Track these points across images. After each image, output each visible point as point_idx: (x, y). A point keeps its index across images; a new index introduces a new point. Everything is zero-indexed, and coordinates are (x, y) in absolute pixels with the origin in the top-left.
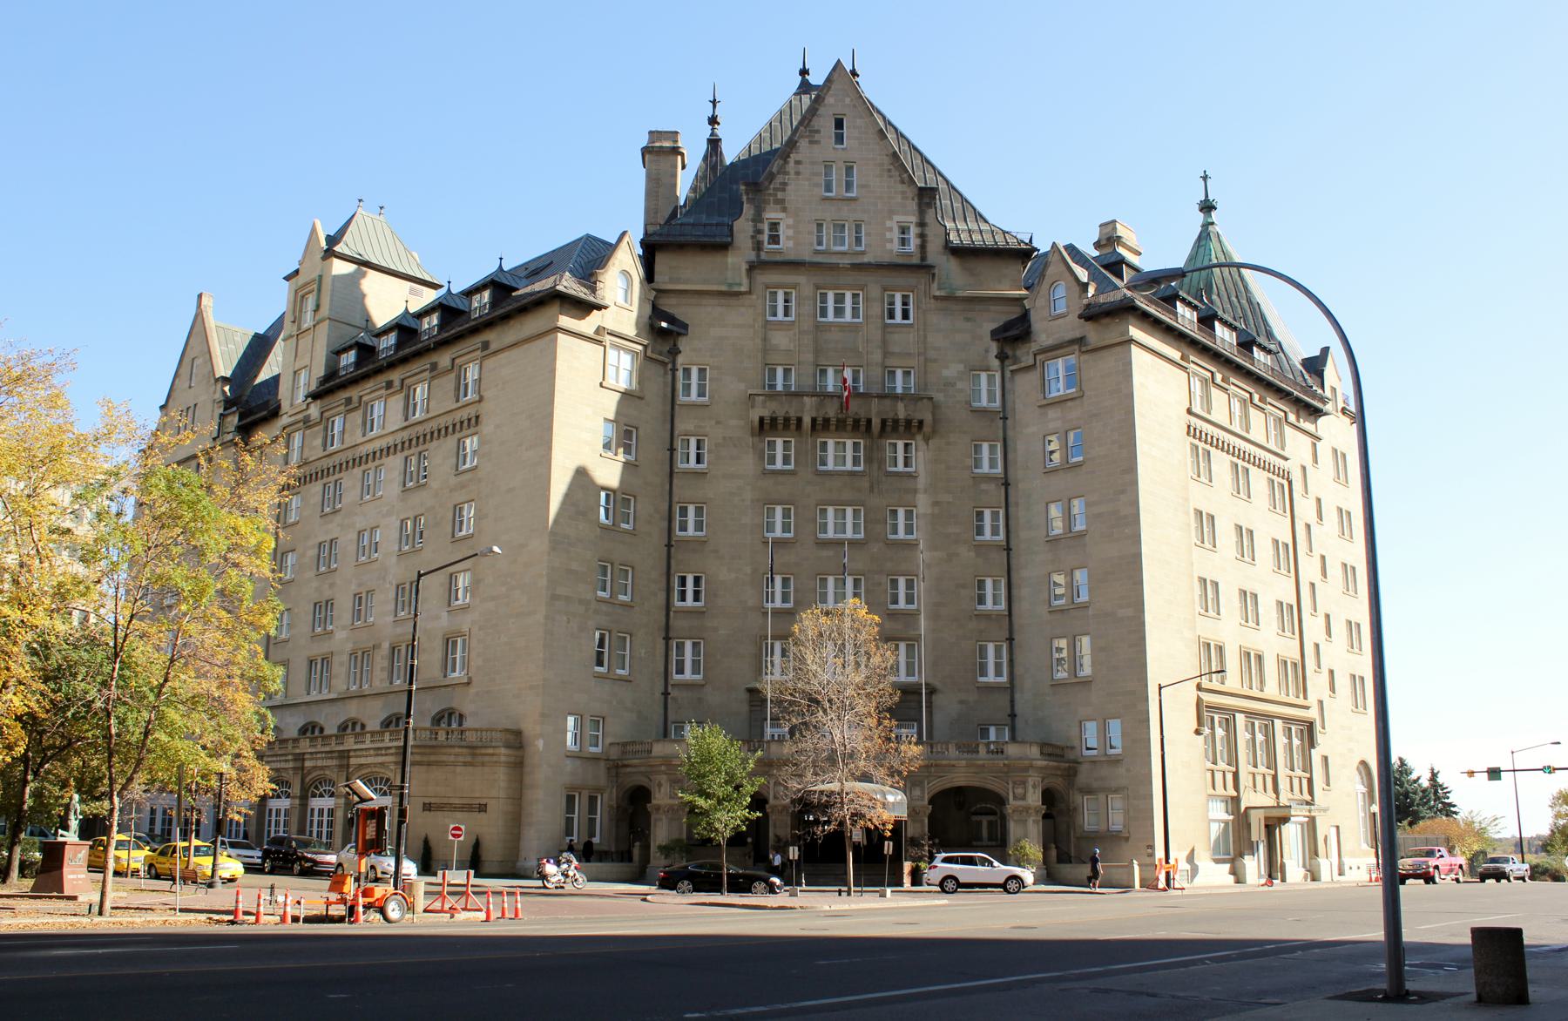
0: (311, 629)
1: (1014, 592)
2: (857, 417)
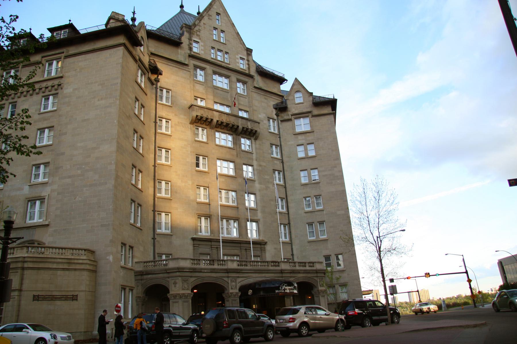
2: (233, 124)
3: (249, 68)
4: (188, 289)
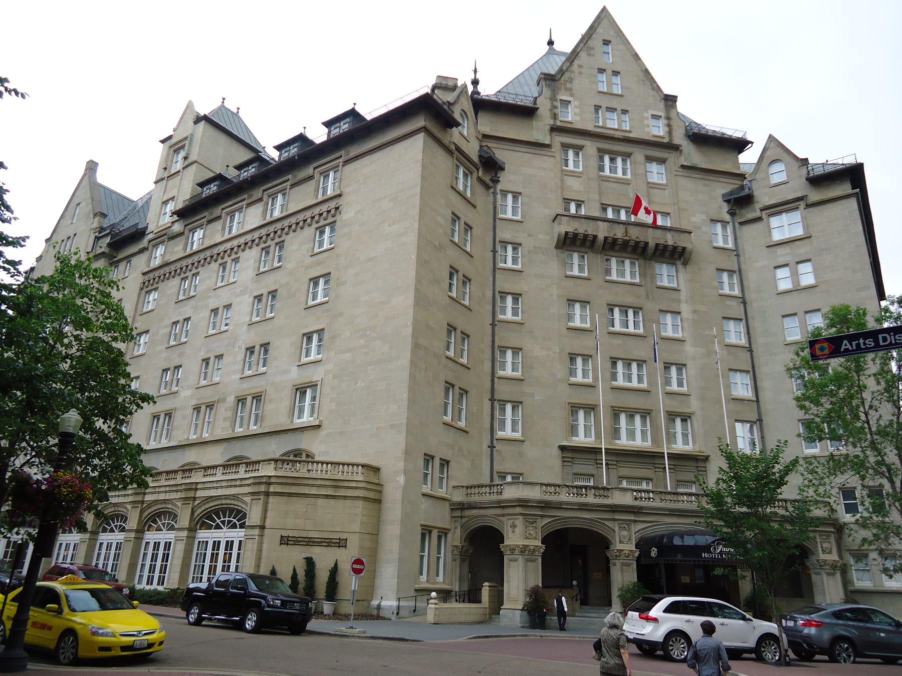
0: (157, 390)
1: (759, 384)
3: (670, 133)
4: (536, 538)
